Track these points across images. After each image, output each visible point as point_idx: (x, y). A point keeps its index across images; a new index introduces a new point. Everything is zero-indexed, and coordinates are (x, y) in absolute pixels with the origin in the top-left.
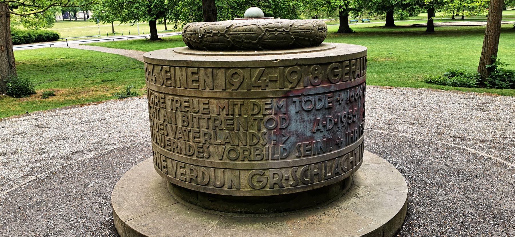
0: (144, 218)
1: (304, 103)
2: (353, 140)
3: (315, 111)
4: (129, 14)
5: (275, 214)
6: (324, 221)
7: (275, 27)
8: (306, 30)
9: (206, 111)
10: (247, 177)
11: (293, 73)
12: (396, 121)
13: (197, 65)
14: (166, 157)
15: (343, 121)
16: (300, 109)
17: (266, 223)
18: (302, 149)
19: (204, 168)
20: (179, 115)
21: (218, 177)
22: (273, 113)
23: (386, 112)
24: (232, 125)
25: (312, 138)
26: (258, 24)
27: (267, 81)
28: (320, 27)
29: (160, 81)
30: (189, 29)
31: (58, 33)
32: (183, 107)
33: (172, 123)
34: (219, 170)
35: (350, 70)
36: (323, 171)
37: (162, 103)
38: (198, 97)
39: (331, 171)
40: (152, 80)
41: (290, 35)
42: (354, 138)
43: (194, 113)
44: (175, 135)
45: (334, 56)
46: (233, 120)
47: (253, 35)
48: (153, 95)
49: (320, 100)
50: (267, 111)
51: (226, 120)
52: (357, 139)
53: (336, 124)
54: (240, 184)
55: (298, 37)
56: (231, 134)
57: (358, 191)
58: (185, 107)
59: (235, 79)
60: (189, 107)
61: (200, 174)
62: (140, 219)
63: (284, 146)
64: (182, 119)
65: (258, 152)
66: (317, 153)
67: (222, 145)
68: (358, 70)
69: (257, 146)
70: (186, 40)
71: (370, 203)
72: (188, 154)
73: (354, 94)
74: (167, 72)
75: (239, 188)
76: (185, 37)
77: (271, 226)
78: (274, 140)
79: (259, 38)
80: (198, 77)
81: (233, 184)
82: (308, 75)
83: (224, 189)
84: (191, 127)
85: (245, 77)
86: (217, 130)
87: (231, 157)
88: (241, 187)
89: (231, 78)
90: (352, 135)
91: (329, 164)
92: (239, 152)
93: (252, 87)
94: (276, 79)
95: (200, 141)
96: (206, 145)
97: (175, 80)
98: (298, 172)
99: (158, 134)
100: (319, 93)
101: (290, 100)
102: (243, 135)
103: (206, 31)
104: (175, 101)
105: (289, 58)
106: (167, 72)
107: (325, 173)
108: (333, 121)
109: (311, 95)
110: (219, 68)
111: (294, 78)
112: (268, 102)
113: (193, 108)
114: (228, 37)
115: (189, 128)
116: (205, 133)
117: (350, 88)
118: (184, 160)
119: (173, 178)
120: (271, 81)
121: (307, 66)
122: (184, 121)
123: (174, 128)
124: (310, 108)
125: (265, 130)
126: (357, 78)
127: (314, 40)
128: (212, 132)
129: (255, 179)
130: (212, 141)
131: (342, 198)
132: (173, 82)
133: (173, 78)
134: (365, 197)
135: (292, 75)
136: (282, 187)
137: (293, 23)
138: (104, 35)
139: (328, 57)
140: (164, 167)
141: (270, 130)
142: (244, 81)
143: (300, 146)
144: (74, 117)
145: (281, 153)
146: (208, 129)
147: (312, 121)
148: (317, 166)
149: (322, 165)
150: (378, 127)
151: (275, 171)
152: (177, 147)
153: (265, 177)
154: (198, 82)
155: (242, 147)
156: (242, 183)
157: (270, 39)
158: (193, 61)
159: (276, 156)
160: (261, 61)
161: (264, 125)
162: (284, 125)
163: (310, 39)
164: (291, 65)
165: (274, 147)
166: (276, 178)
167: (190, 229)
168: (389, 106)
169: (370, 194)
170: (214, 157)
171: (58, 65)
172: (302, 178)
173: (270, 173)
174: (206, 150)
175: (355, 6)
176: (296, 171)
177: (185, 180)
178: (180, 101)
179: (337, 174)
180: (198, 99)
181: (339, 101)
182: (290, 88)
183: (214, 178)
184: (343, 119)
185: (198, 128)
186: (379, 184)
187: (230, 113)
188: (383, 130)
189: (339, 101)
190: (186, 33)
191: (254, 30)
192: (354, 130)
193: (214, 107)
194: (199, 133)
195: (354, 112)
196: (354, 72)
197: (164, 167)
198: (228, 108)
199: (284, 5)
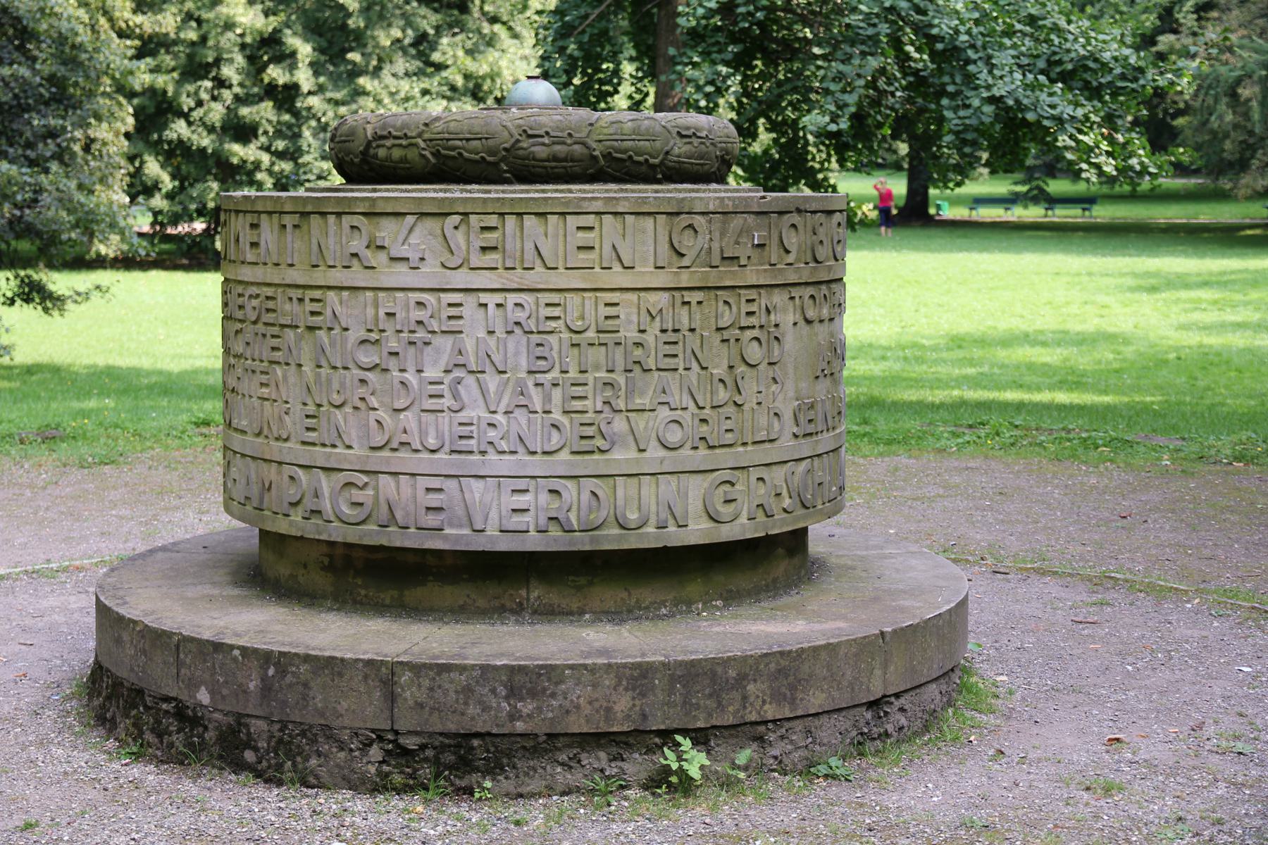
128: (620, 379)
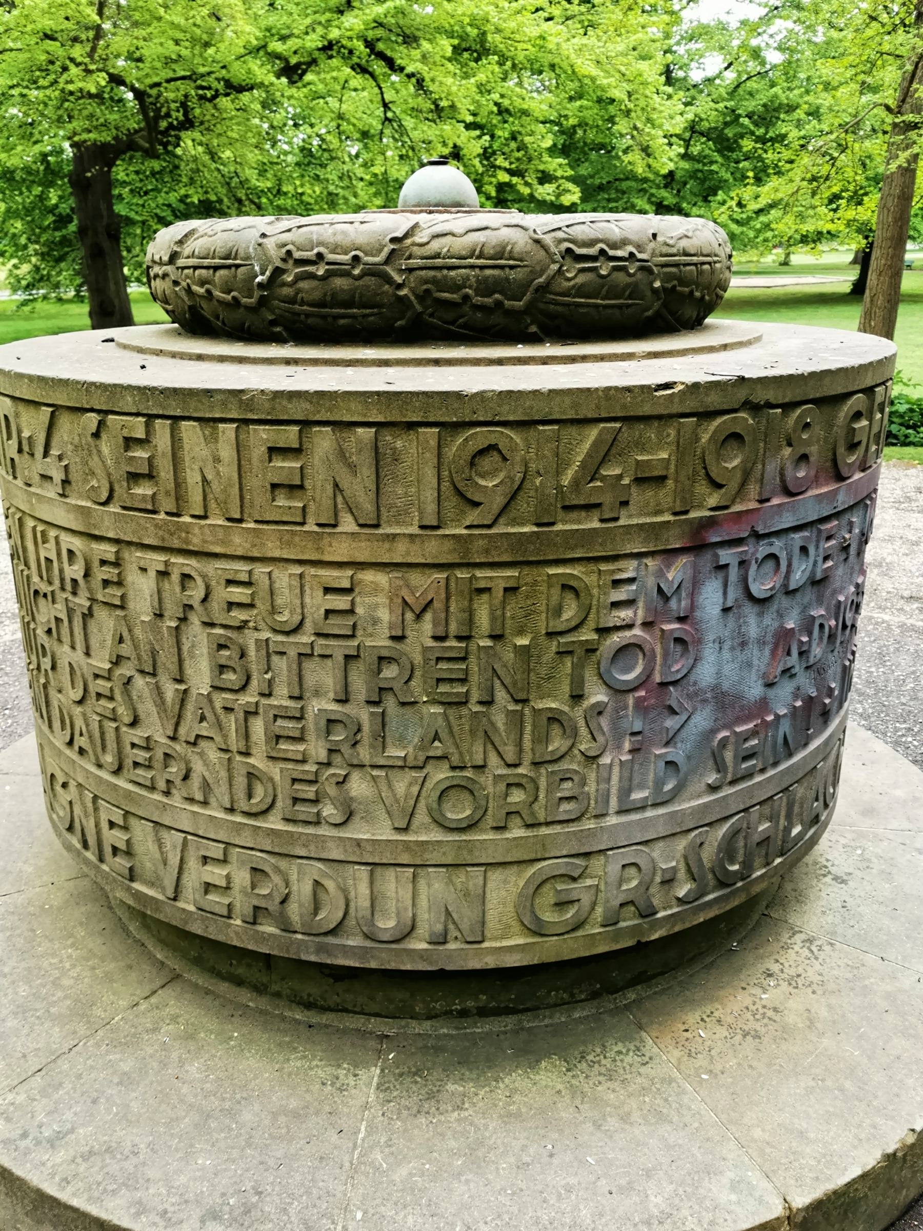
0: (44, 1092)
5: (595, 1003)
7: (598, 241)
9: (337, 625)
13: (297, 411)
14: (127, 812)
18: (729, 755)
19: (319, 865)
21: (384, 897)
24: (148, 673)
25: (763, 705)
29: (94, 483)
30: (195, 246)
32: (216, 605)
33: (160, 671)
34: (391, 873)
38: (301, 562)
40: (46, 478)
43: (275, 631)
44: (177, 724)
47: (512, 275)
48: (51, 545)
50: (615, 613)
51: (433, 663)
54: (483, 923)
56: (451, 718)
59: (483, 476)
61: (303, 889)
69: (564, 765)
70: (183, 294)
72: (243, 805)
74: (130, 442)
75: (480, 939)
76: (176, 283)
77: (603, 1070)
78: (633, 734)
80: (301, 468)
81: (454, 923)
85: (533, 466)
86: (390, 703)
87: (449, 815)
88: (486, 932)
92: (487, 796)
93: (559, 510)
95: (304, 753)
96: (332, 771)
97: (179, 484)
99: (84, 715)
103: (289, 253)
104: (175, 577)
106: (130, 442)
109: (777, 533)
110: (412, 426)
112: (625, 576)
114: (399, 279)
115: (249, 698)
118: (222, 832)
119: (160, 897)
120: (639, 481)
121: (779, 410)
124: (771, 589)
125: (598, 695)
128: (364, 715)
129: (548, 896)
130: (364, 754)
131: (788, 886)
132: (167, 493)
133: (165, 472)
134: (857, 872)
136: (650, 911)
140: (115, 850)
141: (619, 691)
142: (527, 485)
143: (724, 743)
146: (343, 701)
147: (769, 638)
152: (186, 778)
153: (589, 882)
154: (298, 493)
155: (500, 772)
156: (492, 916)
157: (580, 291)
158: (278, 395)
160: (609, 393)
162: (675, 668)
164: (726, 407)
165: (632, 760)
166: (630, 880)
170: (369, 818)
173: (609, 869)
174: (332, 790)
177: (225, 913)
178: (204, 577)
180: (297, 570)
183: (367, 904)
187: (453, 628)
190: (181, 262)
193: (377, 606)
194: (301, 718)
197: (115, 850)
198: (447, 608)
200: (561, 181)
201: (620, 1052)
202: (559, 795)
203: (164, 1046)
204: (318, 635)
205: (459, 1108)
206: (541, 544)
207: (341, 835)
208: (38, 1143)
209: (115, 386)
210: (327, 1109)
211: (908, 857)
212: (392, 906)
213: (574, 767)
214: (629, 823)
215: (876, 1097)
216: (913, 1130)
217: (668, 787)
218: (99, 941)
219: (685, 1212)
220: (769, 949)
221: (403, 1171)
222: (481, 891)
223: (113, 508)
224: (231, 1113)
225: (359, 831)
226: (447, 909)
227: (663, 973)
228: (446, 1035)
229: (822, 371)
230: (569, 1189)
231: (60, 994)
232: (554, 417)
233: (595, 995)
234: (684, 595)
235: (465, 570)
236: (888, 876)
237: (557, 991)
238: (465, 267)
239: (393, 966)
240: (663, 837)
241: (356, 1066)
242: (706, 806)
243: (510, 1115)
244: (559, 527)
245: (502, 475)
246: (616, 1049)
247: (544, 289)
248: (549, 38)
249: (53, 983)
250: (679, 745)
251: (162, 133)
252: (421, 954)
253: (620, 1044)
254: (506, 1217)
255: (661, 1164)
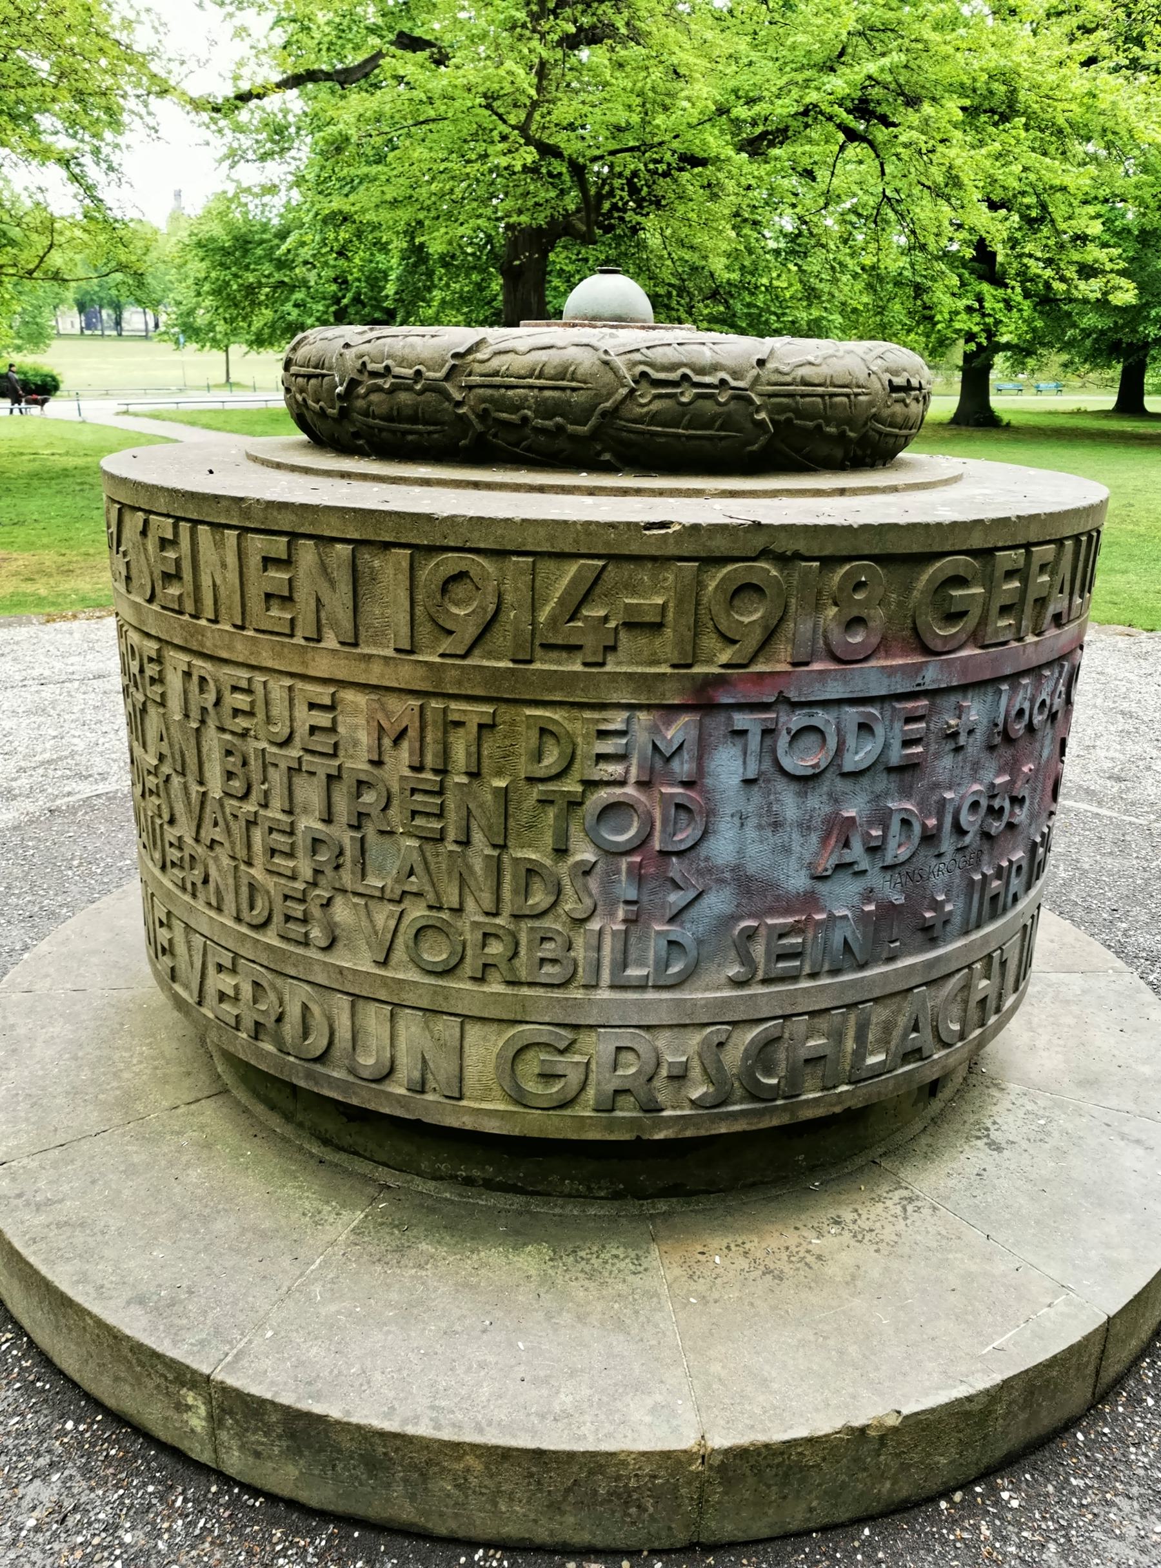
0: (55, 1165)
1: (788, 738)
2: (996, 906)
3: (838, 780)
4: (274, 323)
5: (617, 1204)
6: (831, 1269)
8: (831, 389)
9: (322, 743)
10: (496, 1050)
11: (746, 596)
12: (1149, 768)
13: (285, 522)
15: (965, 827)
16: (767, 765)
17: (570, 1247)
18: (759, 950)
19: (307, 988)
20: (213, 741)
22: (632, 779)
23: (1112, 728)
24: (434, 815)
25: (810, 901)
26: (603, 345)
27: (612, 624)
28: (899, 381)
31: (55, 373)
32: (226, 710)
33: (188, 772)
34: (373, 1007)
35: (1023, 591)
36: (850, 1045)
37: (153, 680)
38: (292, 675)
39: (884, 1042)
41: (751, 409)
42: (1006, 896)
44: (199, 827)
45: (954, 524)
46: (440, 793)
47: (575, 397)
49: (865, 728)
50: (602, 766)
51: (408, 793)
52: (1015, 899)
53: (929, 838)
54: (461, 1080)
55: (789, 421)
56: (428, 854)
57: (995, 1109)
58: (236, 712)
59: (457, 604)
60: (251, 714)
61: (294, 1011)
62: (36, 1164)
63: (675, 931)
64: (222, 763)
65: (549, 949)
66: (826, 967)
67: (390, 900)
68: (1061, 592)
69: (547, 923)
71: (1048, 1181)
73: (1026, 706)
74: (164, 543)
75: (457, 1095)
77: (588, 1268)
78: (627, 902)
79: (604, 414)
80: (290, 580)
82: (818, 607)
83: (390, 1089)
84: (261, 805)
85: (509, 598)
86: (370, 830)
87: (425, 956)
88: (464, 1090)
89: (439, 596)
90: (996, 883)
91: (879, 1014)
93: (538, 650)
94: (658, 620)
95: (294, 869)
96: (317, 892)
97: (197, 587)
98: (729, 1047)
100: (861, 695)
101: (717, 724)
102: (487, 868)
103: (364, 364)
104: (195, 678)
105: (727, 521)
107: (855, 1052)
108: (917, 829)
109: (825, 704)
110: (387, 546)
111: (746, 620)
113: (269, 720)
114: (458, 396)
115: (250, 807)
116: (315, 841)
117: (1014, 678)
120: (629, 626)
122: (230, 775)
123: (194, 795)
124: (813, 767)
125: (585, 854)
126: (1052, 632)
127: (864, 440)
128: (347, 838)
129: (532, 1064)
130: (347, 878)
131: (924, 1140)
134: (1025, 1144)
135: (736, 602)
136: (652, 1106)
137: (772, 352)
138: (197, 388)
139: (927, 525)
141: (612, 853)
142: (502, 617)
143: (750, 935)
144: (9, 658)
145: (657, 963)
147: (817, 822)
148: (823, 1023)
149: (845, 1020)
150: (1080, 787)
151: (625, 1038)
152: (206, 881)
153: (577, 1058)
154: (288, 605)
156: (471, 1073)
157: (654, 418)
158: (270, 505)
159: (633, 972)
160: (588, 526)
161: (585, 830)
163: (844, 432)
164: (736, 553)
165: (626, 931)
167: (230, 1248)
168: (1125, 705)
169: (1049, 1134)
170: (352, 949)
171: (36, 475)
172: (748, 1074)
174: (316, 912)
175: (1020, 337)
176: (721, 1045)
178: (216, 681)
179: (916, 1054)
180: (288, 682)
181: (955, 735)
182: (723, 666)
183: (348, 1035)
184: (966, 819)
185: (290, 812)
186: (1089, 1083)
187: (429, 760)
188: (1100, 804)
189: (955, 735)
191: (580, 371)
192: (1011, 862)
194: (291, 833)
195: (1019, 783)
196: (1042, 602)
198: (422, 739)
199: (778, 321)
200: (1110, 276)
201: (616, 1256)
202: (540, 954)
203: (180, 1149)
204: (306, 750)
205: (420, 1267)
206: (516, 681)
207: (327, 960)
208: (28, 1204)
209: (154, 486)
210: (295, 1236)
211: (1104, 1139)
212: (373, 1043)
213: (559, 927)
214: (625, 1001)
215: (877, 1369)
216: (899, 1412)
217: (674, 969)
218: (175, 1045)
219: (588, 1418)
220: (855, 1196)
221: (333, 1308)
222: (458, 1044)
223: (155, 607)
224: (205, 1220)
225: (341, 959)
226: (423, 1057)
227: (709, 1192)
228: (446, 1199)
229: (881, 525)
230: (482, 1365)
231: (115, 1084)
232: (528, 548)
233: (616, 1196)
234: (686, 757)
235: (440, 700)
236: (1060, 1153)
237: (572, 1179)
238: (523, 387)
239: (372, 1106)
240: (670, 1026)
241: (343, 1206)
242: (724, 1000)
243: (466, 1285)
244: (537, 666)
245: (475, 604)
246: (614, 1252)
247: (614, 412)
248: (1101, 96)
249: (115, 1074)
250: (688, 925)
251: (603, 215)
252: (399, 1099)
253: (622, 1249)
254: (405, 1373)
255: (591, 1368)
